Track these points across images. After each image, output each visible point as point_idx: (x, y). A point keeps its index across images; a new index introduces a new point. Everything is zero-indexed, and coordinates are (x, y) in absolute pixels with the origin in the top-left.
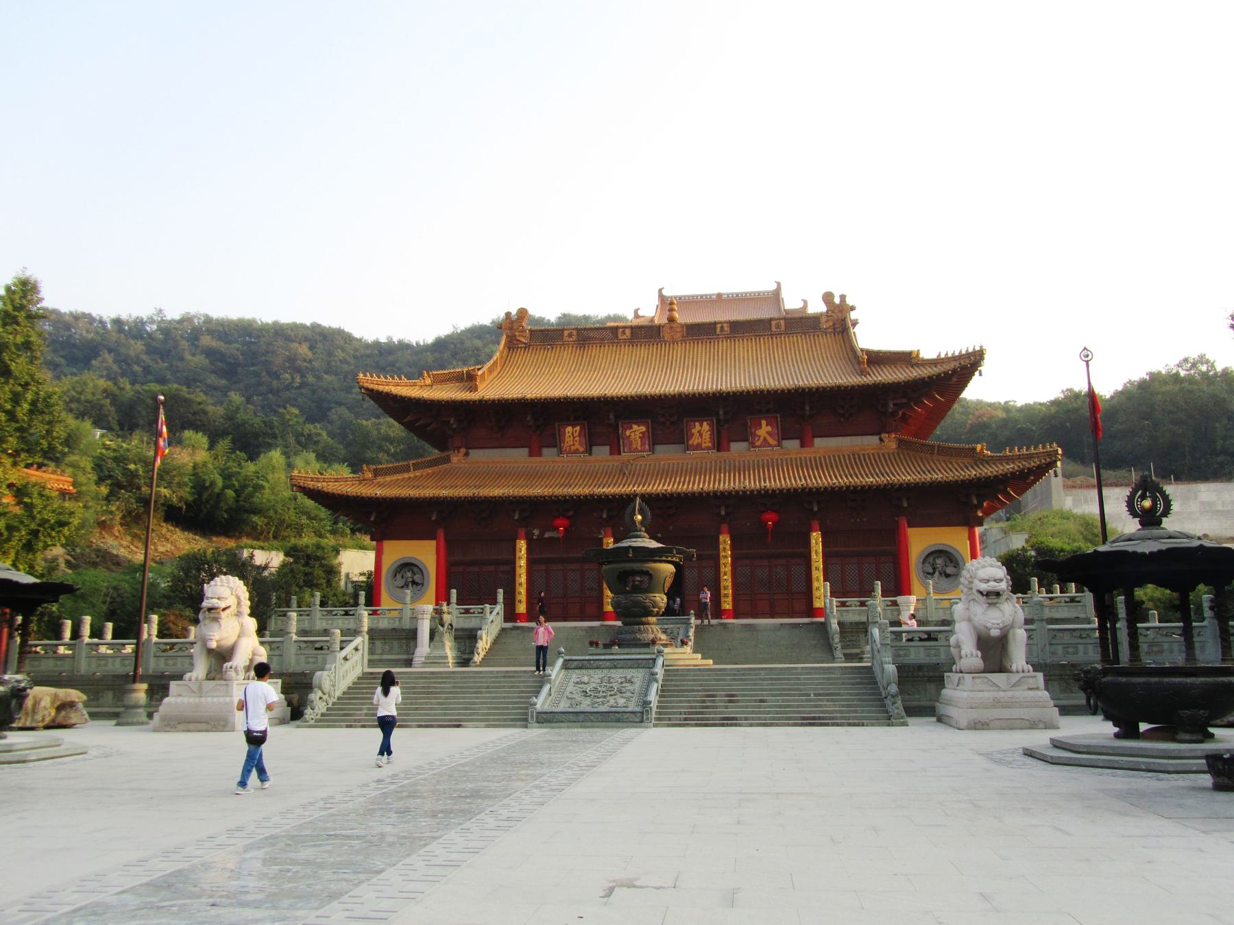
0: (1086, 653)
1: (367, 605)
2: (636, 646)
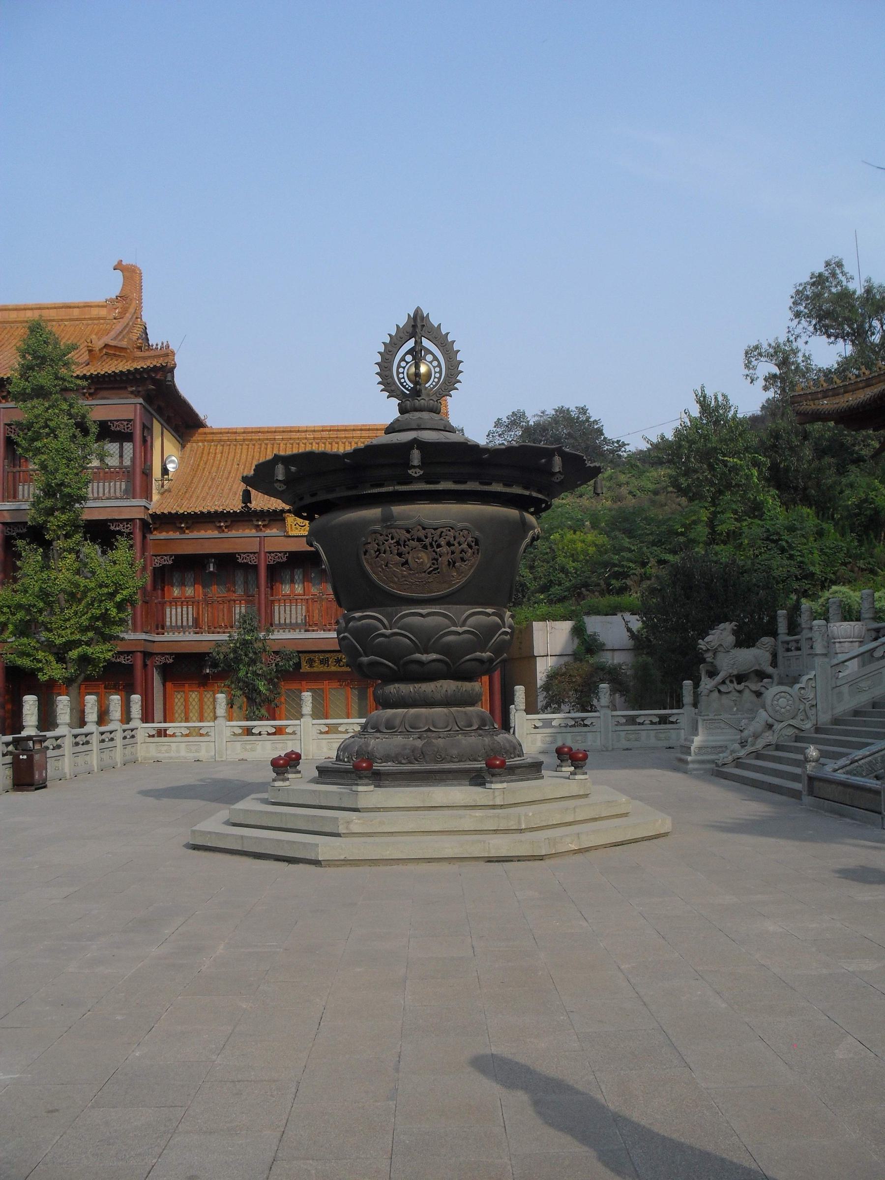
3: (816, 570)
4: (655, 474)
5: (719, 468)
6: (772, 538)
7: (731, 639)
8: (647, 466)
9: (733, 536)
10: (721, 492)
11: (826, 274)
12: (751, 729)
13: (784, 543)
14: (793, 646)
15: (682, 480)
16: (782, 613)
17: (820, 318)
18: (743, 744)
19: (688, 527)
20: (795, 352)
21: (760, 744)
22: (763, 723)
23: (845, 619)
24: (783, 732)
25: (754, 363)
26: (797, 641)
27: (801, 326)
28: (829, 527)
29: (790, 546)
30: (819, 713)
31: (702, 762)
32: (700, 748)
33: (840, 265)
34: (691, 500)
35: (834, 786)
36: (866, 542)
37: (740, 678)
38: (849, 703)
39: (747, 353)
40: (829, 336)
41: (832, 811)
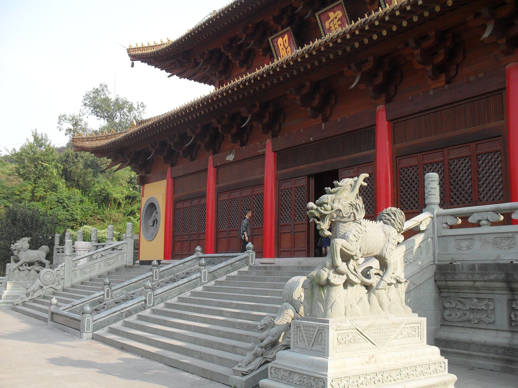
3: (78, 217)
4: (10, 166)
5: (40, 167)
6: (60, 201)
7: (28, 245)
8: (7, 162)
9: (42, 198)
10: (39, 178)
11: (100, 89)
12: (32, 288)
13: (65, 204)
14: (61, 250)
15: (21, 170)
16: (57, 235)
17: (95, 108)
18: (28, 295)
19: (21, 192)
20: (81, 120)
21: (36, 295)
22: (38, 286)
23: (84, 240)
24: (47, 290)
25: (62, 122)
26: (63, 249)
27: (86, 110)
28: (86, 199)
29: (68, 206)
30: (65, 282)
31: (7, 303)
32: (7, 296)
33: (106, 86)
34: (25, 180)
35: (62, 317)
36: (101, 207)
37: (31, 264)
38: (80, 278)
39: (59, 117)
40: (98, 116)
41: (60, 329)
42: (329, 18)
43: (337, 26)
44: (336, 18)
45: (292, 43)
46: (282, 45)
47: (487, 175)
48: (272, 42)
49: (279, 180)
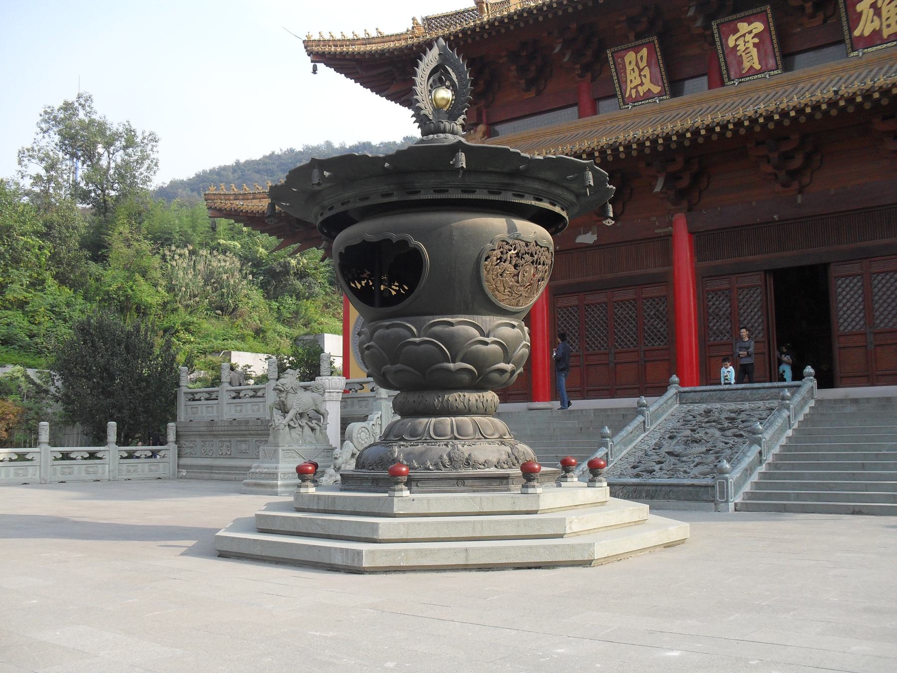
0: (7, 476)
1: (119, 443)
2: (461, 481)
25: (26, 162)
33: (89, 99)
42: (736, 30)
43: (750, 45)
44: (750, 32)
45: (653, 61)
46: (634, 63)
47: (752, 299)
48: (612, 56)
49: (702, 278)
